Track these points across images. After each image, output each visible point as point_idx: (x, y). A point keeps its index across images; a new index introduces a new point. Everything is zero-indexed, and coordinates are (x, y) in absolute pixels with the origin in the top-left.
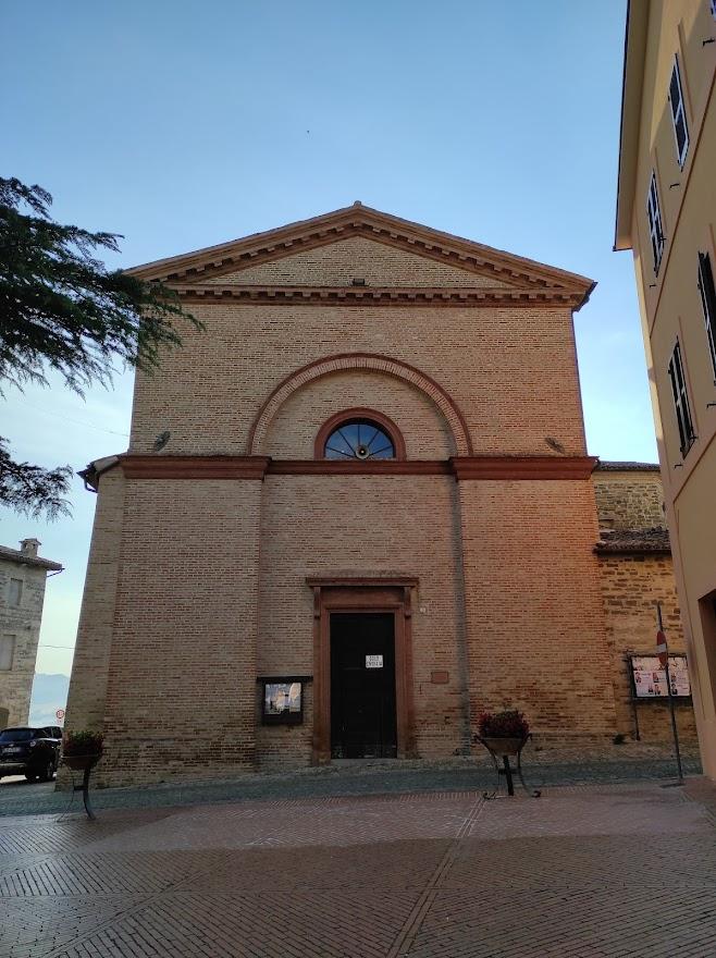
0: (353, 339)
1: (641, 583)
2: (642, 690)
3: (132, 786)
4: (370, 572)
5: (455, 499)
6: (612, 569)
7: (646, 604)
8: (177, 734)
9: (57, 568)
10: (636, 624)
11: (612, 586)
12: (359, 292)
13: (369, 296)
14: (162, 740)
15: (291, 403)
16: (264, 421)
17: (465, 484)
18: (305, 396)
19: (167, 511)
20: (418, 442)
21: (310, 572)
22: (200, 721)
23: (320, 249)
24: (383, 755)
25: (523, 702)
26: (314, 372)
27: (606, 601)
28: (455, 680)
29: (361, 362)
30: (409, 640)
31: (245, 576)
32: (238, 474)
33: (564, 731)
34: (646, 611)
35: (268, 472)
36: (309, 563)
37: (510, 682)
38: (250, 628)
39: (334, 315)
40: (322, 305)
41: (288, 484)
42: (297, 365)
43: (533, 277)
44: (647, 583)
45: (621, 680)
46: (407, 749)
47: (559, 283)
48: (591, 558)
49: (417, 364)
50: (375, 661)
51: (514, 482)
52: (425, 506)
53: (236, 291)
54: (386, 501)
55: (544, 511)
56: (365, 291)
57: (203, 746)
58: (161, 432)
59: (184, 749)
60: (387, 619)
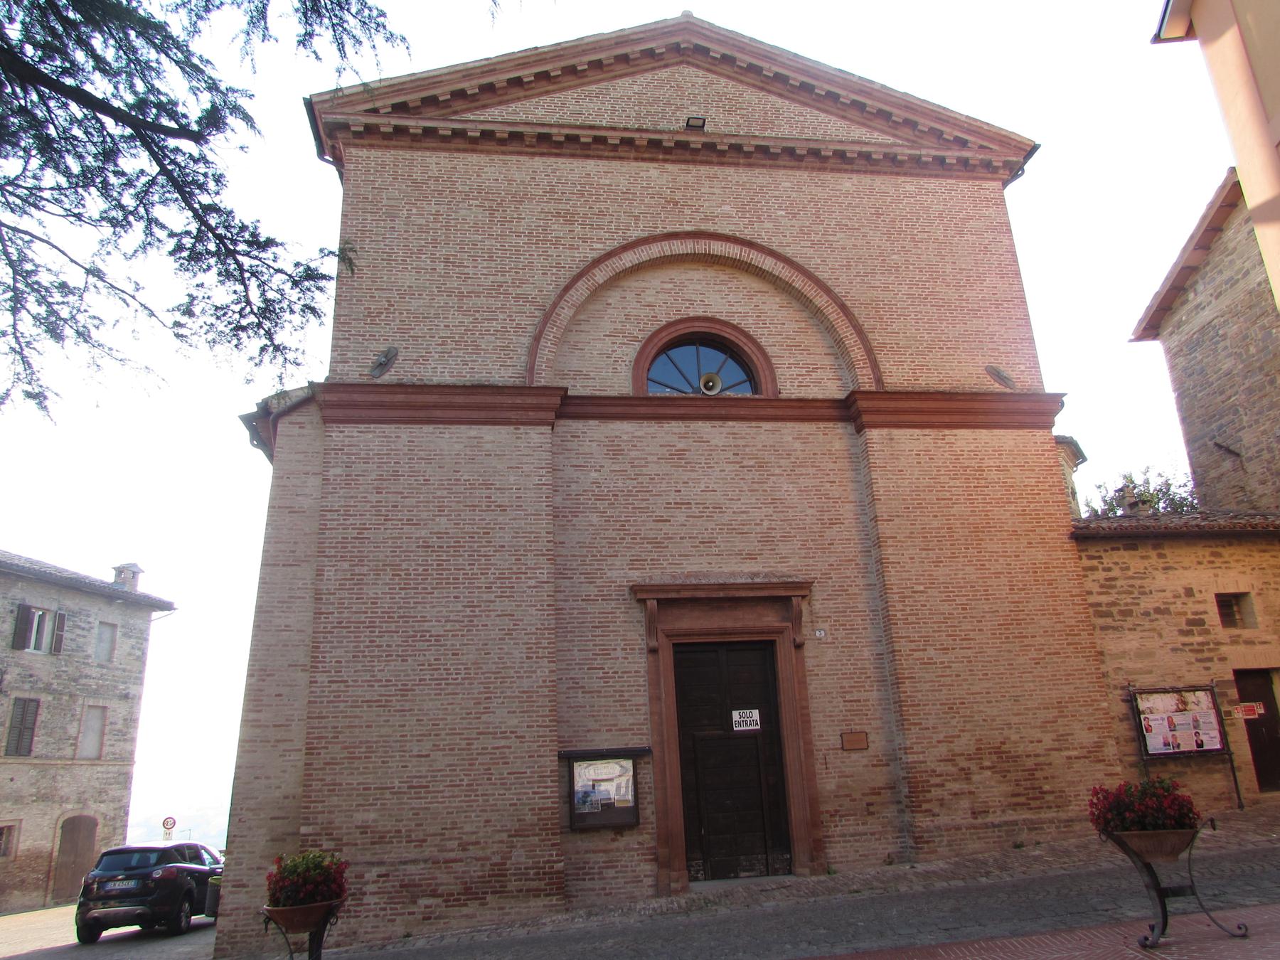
0: (687, 211)
1: (1137, 583)
2: (1155, 743)
3: (355, 946)
4: (733, 574)
5: (860, 460)
6: (1095, 562)
7: (1147, 614)
8: (429, 851)
9: (166, 606)
10: (1135, 644)
11: (1096, 589)
12: (695, 140)
13: (710, 147)
14: (405, 863)
15: (591, 307)
16: (551, 333)
17: (874, 434)
18: (614, 297)
19: (396, 475)
20: (795, 371)
21: (636, 576)
22: (468, 828)
23: (629, 80)
24: (769, 871)
25: (988, 773)
26: (629, 259)
27: (1091, 610)
28: (877, 743)
29: (702, 247)
30: (803, 684)
31: (532, 582)
32: (513, 415)
33: (1051, 814)
34: (1147, 625)
35: (560, 415)
36: (634, 563)
37: (965, 743)
38: (544, 670)
39: (655, 175)
40: (636, 159)
41: (593, 434)
42: (600, 248)
43: (949, 133)
44: (1146, 582)
45: (1123, 729)
46: (812, 860)
47: (985, 144)
48: (1067, 546)
49: (789, 252)
50: (746, 720)
51: (947, 432)
52: (811, 471)
53: (502, 131)
54: (752, 463)
55: (993, 475)
56: (704, 139)
57: (475, 870)
58: (383, 348)
59: (442, 876)
60: (764, 649)
